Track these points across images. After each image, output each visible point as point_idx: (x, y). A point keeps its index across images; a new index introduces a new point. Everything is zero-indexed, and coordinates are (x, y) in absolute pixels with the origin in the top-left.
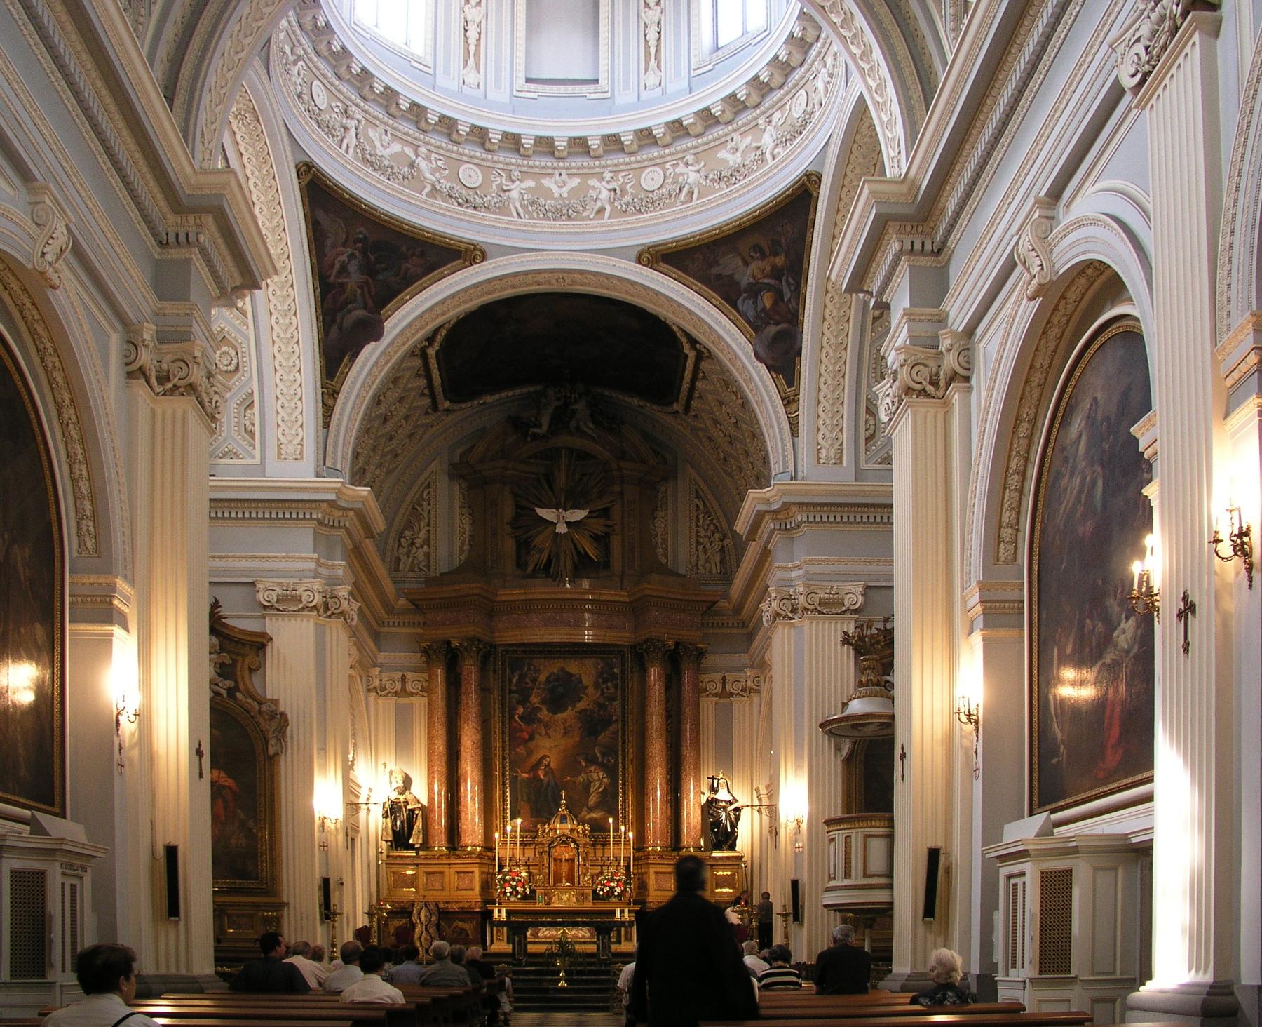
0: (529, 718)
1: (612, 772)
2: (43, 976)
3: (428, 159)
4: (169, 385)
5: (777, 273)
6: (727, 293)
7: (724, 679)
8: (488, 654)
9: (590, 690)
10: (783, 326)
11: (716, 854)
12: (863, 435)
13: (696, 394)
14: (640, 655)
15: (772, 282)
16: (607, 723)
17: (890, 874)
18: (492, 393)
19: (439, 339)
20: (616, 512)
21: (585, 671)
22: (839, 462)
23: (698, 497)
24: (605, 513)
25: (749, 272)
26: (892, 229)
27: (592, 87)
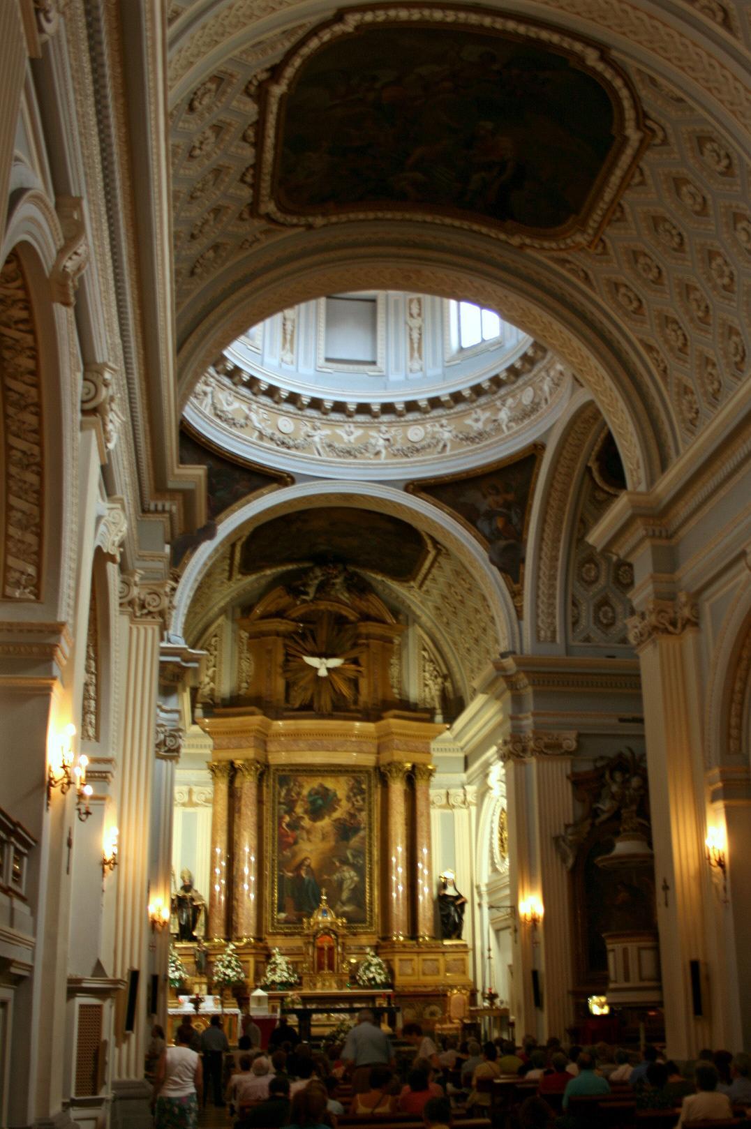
0: (295, 825)
1: (360, 870)
2: (95, 1093)
3: (257, 413)
4: (145, 611)
5: (507, 505)
6: (469, 516)
7: (448, 794)
8: (264, 771)
9: (344, 803)
10: (512, 541)
11: (447, 942)
12: (570, 620)
13: (430, 576)
14: (382, 775)
15: (505, 511)
16: (356, 830)
17: (658, 977)
18: (270, 567)
19: (289, 72)
20: (363, 659)
21: (339, 787)
22: (553, 639)
23: (425, 649)
24: (356, 662)
25: (486, 503)
26: (639, 522)
27: (371, 367)
